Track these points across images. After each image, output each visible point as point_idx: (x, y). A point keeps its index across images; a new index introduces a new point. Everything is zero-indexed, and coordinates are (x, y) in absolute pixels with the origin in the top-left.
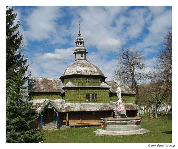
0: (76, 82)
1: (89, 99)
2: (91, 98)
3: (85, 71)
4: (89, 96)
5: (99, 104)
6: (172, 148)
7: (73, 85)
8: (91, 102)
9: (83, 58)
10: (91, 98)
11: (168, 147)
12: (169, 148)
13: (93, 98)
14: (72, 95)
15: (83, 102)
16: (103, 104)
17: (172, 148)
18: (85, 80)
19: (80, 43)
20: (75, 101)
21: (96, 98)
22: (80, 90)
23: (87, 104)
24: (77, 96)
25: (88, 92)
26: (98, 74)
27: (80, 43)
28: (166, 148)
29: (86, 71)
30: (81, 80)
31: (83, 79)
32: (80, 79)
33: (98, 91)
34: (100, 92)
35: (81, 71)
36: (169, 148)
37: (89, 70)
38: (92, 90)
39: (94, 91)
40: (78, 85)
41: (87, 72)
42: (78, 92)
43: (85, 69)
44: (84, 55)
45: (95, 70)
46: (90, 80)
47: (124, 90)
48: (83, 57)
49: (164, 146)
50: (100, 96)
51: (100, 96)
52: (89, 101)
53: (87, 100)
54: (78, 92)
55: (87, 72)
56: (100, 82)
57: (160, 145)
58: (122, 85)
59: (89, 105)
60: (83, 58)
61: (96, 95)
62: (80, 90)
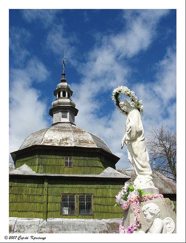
0: (39, 165)
1: (72, 207)
2: (77, 206)
3: (63, 140)
4: (72, 199)
5: (97, 221)
6: (41, 241)
7: (34, 173)
8: (77, 217)
9: (67, 120)
10: (77, 206)
11: (35, 239)
12: (36, 241)
13: (82, 207)
14: (25, 197)
15: (54, 217)
16: (108, 221)
17: (41, 241)
18: (62, 160)
19: (61, 93)
20: (32, 213)
21: (89, 206)
22: (46, 184)
23: (66, 220)
24: (39, 199)
25: (67, 189)
26: (95, 146)
27: (61, 93)
28: (32, 241)
29: (66, 139)
30: (52, 160)
31: (58, 157)
32: (49, 157)
33: (95, 186)
34: (100, 191)
35: (52, 139)
36: (36, 241)
37: (72, 139)
38: (79, 186)
39: (84, 186)
40: (44, 172)
41: (68, 141)
42: (43, 190)
43: (64, 135)
44: (68, 113)
45: (90, 138)
46: (74, 160)
47: (162, 186)
48: (66, 117)
49: (30, 238)
50: (99, 201)
51: (99, 201)
52: (72, 214)
53: (66, 212)
54: (43, 190)
55: (68, 141)
56: (100, 164)
57: (22, 237)
58: (156, 176)
59: (69, 224)
60: (67, 120)
61: (89, 198)
62: (46, 184)
